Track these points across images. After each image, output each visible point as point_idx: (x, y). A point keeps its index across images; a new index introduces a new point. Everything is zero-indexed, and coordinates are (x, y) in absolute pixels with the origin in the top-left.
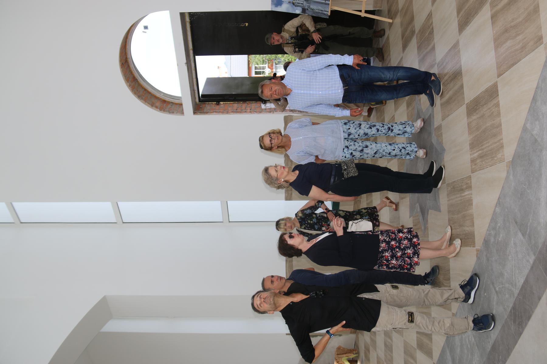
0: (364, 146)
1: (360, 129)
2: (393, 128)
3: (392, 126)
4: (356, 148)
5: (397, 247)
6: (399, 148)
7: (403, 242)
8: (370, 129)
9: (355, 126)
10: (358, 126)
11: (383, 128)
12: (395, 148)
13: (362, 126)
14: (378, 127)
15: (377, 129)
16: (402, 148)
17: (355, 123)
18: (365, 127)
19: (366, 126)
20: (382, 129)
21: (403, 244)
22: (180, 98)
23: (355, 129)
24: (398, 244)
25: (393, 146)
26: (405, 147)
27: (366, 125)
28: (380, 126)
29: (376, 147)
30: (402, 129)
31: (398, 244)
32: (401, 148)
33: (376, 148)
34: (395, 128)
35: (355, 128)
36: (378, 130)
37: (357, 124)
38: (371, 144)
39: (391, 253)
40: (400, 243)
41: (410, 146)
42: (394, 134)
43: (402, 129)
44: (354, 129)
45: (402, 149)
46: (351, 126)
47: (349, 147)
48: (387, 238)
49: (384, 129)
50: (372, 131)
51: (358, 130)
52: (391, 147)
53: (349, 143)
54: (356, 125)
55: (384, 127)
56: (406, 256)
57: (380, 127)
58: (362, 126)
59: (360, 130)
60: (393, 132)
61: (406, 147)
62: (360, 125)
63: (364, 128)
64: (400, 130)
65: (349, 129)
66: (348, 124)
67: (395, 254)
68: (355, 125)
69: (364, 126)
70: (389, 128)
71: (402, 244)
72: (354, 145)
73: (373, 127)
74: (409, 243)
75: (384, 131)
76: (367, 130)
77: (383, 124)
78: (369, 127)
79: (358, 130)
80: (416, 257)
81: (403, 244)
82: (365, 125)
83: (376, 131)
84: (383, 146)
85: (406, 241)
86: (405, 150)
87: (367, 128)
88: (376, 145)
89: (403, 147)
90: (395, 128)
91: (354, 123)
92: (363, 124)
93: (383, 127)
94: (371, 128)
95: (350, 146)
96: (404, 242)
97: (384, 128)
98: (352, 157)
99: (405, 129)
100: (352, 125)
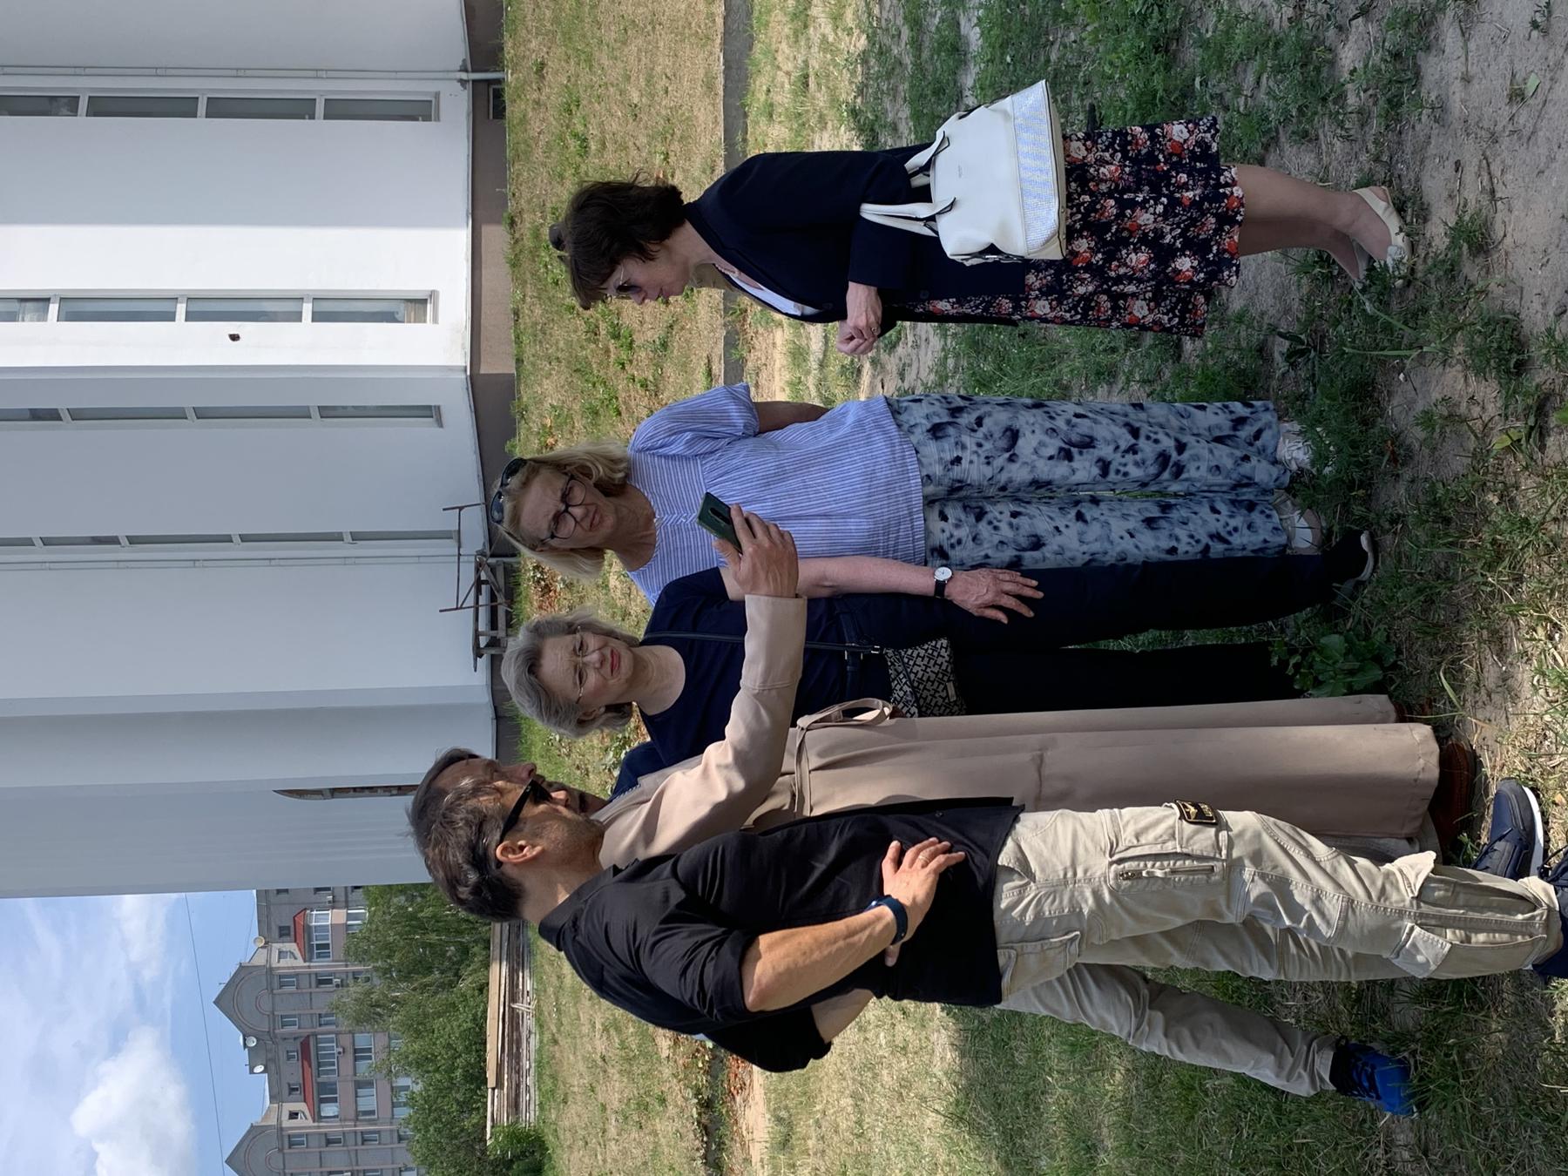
0: (1024, 542)
1: (1011, 459)
2: (1186, 455)
3: (1181, 447)
4: (983, 553)
5: (1089, 267)
6: (1198, 541)
7: (1128, 254)
8: (1066, 462)
9: (988, 446)
10: (1003, 443)
11: (1130, 457)
12: (1177, 539)
13: (1025, 445)
14: (1105, 451)
15: (1100, 460)
16: (1212, 536)
17: (986, 421)
18: (1036, 452)
19: (1042, 444)
20: (1123, 461)
21: (1125, 265)
22: (263, 896)
23: (988, 463)
24: (1100, 256)
25: (1167, 533)
26: (1223, 534)
27: (1046, 439)
28: (1117, 448)
29: (1082, 542)
30: (1228, 463)
31: (1100, 256)
32: (1205, 540)
33: (1085, 548)
34: (1196, 458)
35: (987, 458)
36: (1105, 466)
37: (997, 435)
38: (1057, 528)
39: (1049, 278)
40: (1110, 257)
41: (1249, 527)
42: (1186, 484)
43: (1228, 463)
44: (983, 459)
45: (1211, 543)
46: (964, 447)
47: (951, 553)
48: (1172, 230)
49: (1137, 464)
50: (1074, 471)
51: (1002, 469)
52: (1157, 539)
53: (947, 534)
54: (989, 436)
55: (1135, 453)
56: (1218, 209)
57: (1119, 455)
58: (1021, 442)
59: (1014, 467)
60: (1184, 476)
61: (1230, 533)
62: (1013, 435)
63: (1035, 457)
64: (1218, 467)
65: (958, 460)
66: (951, 430)
67: (1065, 287)
68: (986, 438)
69: (1034, 443)
70: (1163, 459)
71: (1118, 260)
72: (974, 539)
73: (1081, 453)
74: (1152, 266)
75: (1135, 473)
76: (1046, 469)
77: (1135, 432)
78: (1061, 449)
79: (1002, 469)
80: (1160, 209)
81: (1125, 265)
82: (1040, 436)
83: (1096, 471)
84: (1115, 536)
85: (1143, 257)
86: (1226, 546)
87: (1051, 458)
88: (1081, 534)
89: (1214, 531)
90: (1196, 458)
91: (979, 421)
92: (1028, 434)
93: (1133, 450)
94: (1069, 457)
95: (952, 546)
96: (1133, 256)
97: (1138, 457)
98: (972, 519)
99: (1246, 468)
100: (967, 440)
